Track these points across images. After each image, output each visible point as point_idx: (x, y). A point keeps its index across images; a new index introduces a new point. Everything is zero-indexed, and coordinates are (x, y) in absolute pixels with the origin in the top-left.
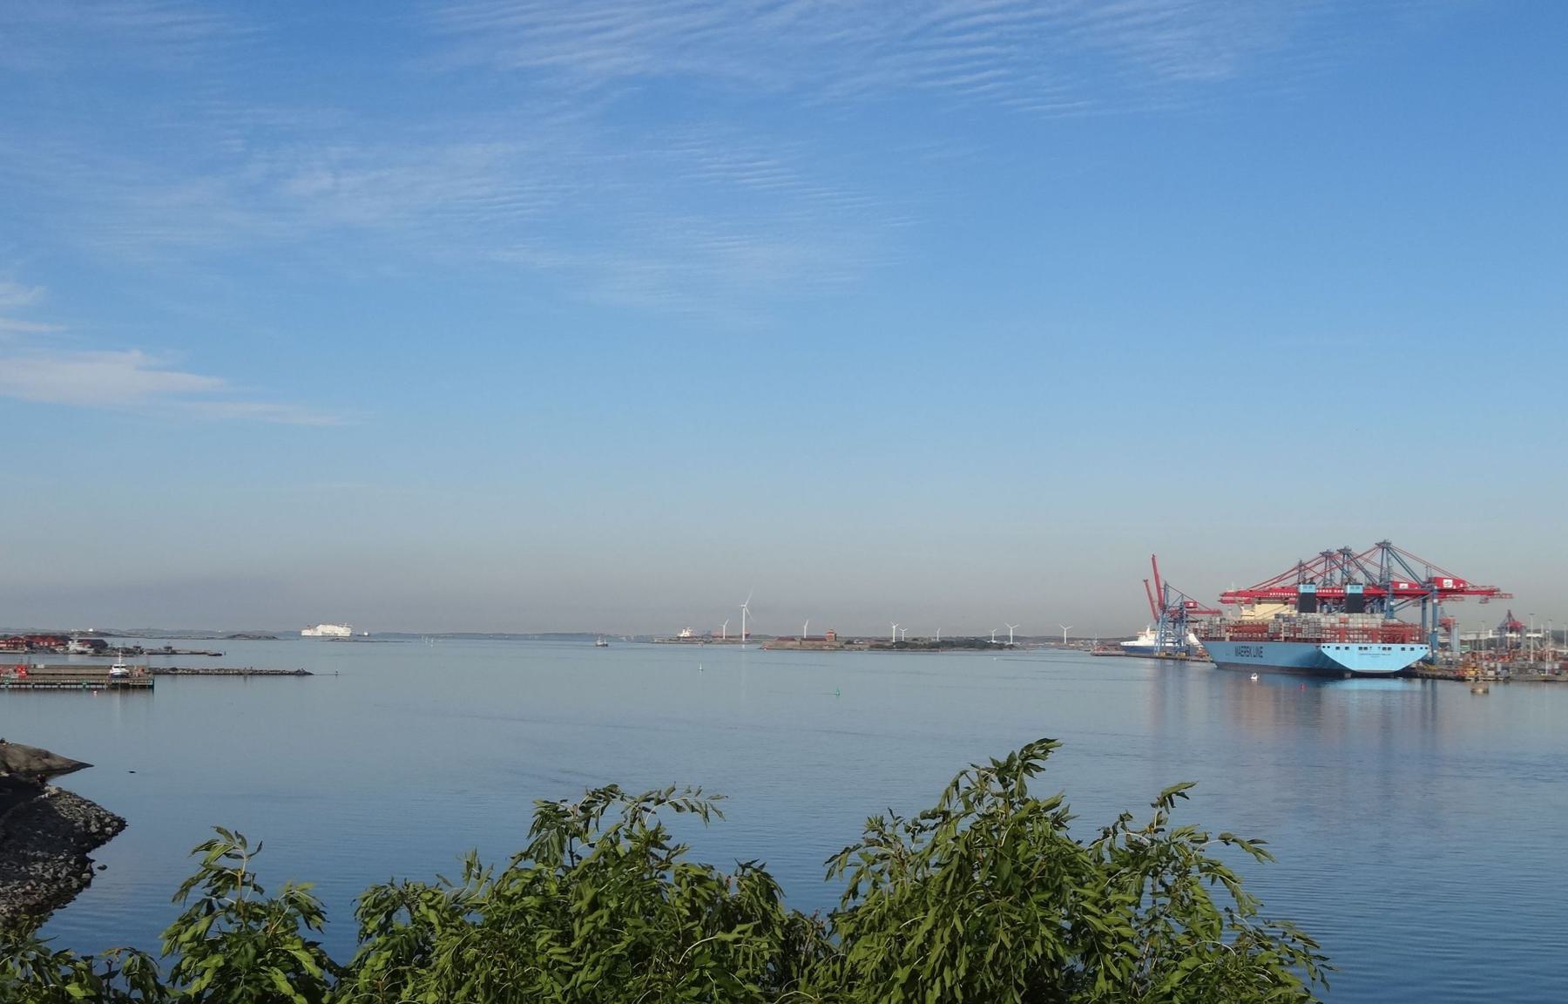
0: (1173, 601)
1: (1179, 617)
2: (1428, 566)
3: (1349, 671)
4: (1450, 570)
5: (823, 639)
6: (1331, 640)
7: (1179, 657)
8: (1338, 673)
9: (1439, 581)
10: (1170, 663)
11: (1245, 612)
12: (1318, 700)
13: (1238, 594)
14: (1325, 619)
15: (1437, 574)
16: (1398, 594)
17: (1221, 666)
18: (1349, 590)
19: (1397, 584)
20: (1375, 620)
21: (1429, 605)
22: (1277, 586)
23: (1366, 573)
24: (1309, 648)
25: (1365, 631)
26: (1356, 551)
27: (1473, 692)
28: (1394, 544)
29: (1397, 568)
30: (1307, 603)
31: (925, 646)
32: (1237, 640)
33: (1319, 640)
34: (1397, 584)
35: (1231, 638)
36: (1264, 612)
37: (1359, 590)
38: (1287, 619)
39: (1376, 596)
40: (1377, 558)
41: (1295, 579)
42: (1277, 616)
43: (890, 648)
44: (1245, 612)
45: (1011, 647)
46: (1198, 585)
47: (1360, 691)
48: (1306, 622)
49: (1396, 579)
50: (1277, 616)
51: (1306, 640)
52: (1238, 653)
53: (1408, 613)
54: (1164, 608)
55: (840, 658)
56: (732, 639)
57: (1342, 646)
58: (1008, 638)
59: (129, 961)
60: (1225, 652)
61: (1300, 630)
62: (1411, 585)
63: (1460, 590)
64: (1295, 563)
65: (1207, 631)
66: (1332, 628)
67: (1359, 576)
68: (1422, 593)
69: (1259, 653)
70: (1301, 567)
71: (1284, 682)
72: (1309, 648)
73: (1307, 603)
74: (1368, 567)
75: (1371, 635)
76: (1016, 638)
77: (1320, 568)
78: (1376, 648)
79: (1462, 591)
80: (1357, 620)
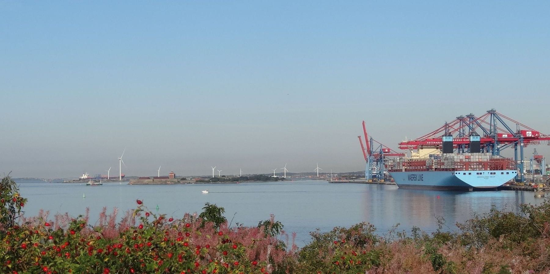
0: (376, 149)
1: (380, 158)
2: (517, 124)
3: (471, 187)
4: (531, 123)
5: (168, 178)
6: (461, 169)
7: (376, 181)
8: (465, 188)
9: (524, 132)
10: (375, 186)
11: (414, 154)
12: (454, 202)
13: (409, 143)
14: (456, 156)
15: (522, 129)
16: (501, 141)
17: (401, 187)
18: (472, 139)
19: (501, 135)
20: (485, 156)
21: (519, 147)
22: (431, 138)
23: (483, 129)
24: (448, 174)
25: (480, 163)
26: (477, 116)
27: (535, 197)
28: (498, 111)
29: (499, 125)
30: (448, 148)
31: (229, 180)
32: (409, 170)
33: (454, 170)
34: (501, 135)
35: (406, 170)
36: (424, 154)
37: (478, 139)
38: (436, 157)
39: (489, 143)
40: (488, 120)
41: (443, 133)
42: (431, 156)
43: (208, 182)
44: (414, 154)
45: (283, 179)
46: (388, 139)
47: (479, 199)
48: (446, 159)
49: (499, 132)
50: (431, 156)
51: (447, 170)
52: (410, 179)
53: (507, 152)
54: (370, 153)
55: (179, 189)
56: (114, 179)
57: (467, 172)
58: (283, 174)
59: (530, 239)
60: (402, 178)
61: (443, 164)
62: (508, 135)
63: (536, 138)
64: (444, 124)
65: (392, 166)
66: (461, 162)
67: (479, 131)
68: (518, 139)
69: (421, 179)
70: (446, 126)
71: (435, 194)
72: (448, 174)
73: (448, 148)
74: (483, 125)
75: (484, 165)
76: (288, 174)
77: (457, 126)
78: (487, 173)
79: (537, 138)
80: (476, 157)
